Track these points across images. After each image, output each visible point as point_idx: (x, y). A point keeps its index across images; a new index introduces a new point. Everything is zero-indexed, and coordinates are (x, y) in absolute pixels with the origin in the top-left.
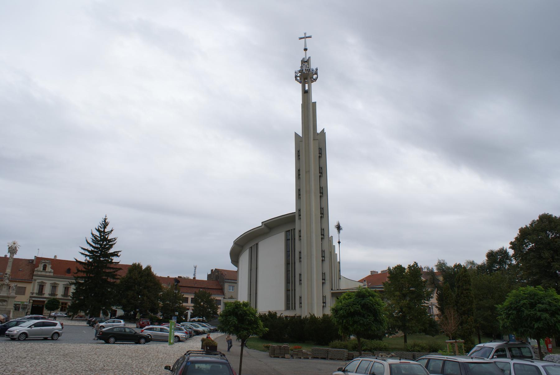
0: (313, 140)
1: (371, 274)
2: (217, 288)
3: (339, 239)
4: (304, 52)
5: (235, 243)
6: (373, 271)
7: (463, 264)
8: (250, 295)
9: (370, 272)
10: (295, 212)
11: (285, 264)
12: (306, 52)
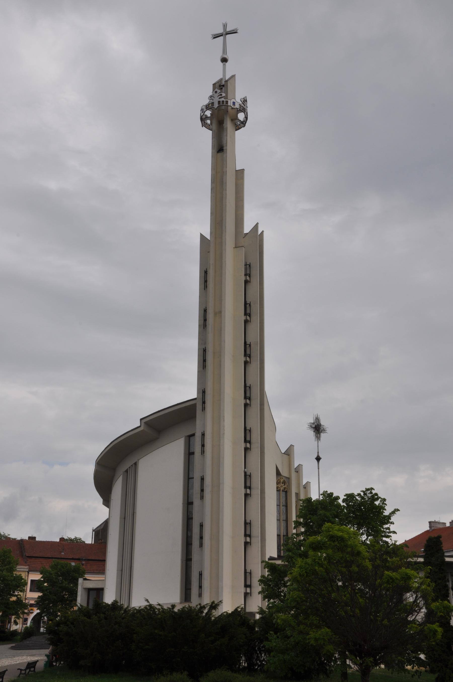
0: (236, 247)
1: (430, 527)
3: (318, 452)
4: (221, 64)
5: (97, 463)
6: (435, 522)
9: (428, 523)
11: (183, 504)
12: (224, 66)
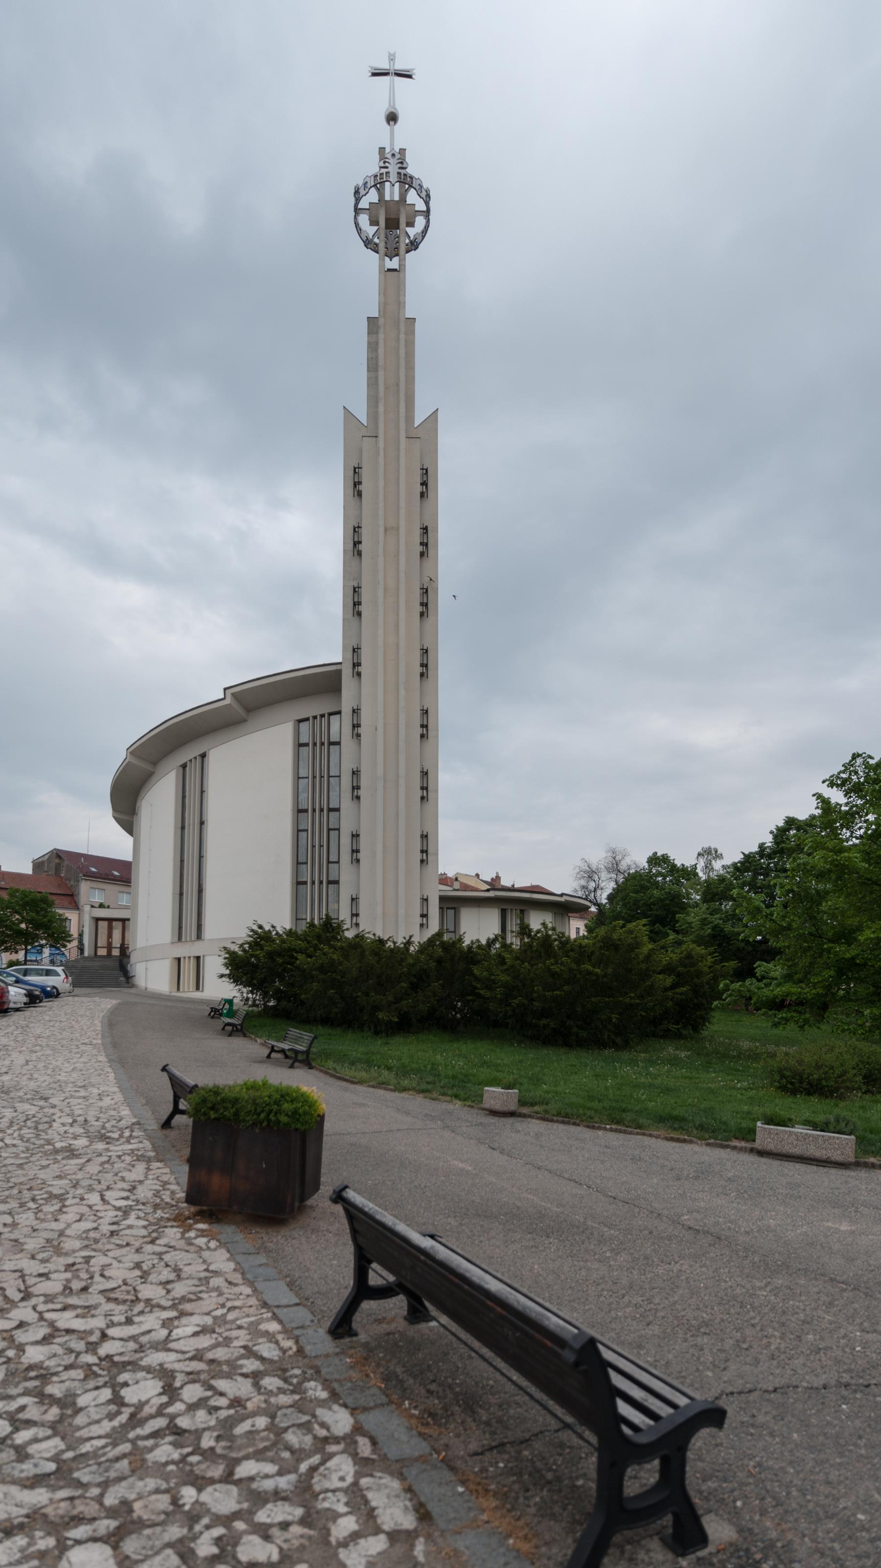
2: (59, 892)
5: (131, 753)
7: (684, 858)
8: (181, 894)
10: (340, 663)
